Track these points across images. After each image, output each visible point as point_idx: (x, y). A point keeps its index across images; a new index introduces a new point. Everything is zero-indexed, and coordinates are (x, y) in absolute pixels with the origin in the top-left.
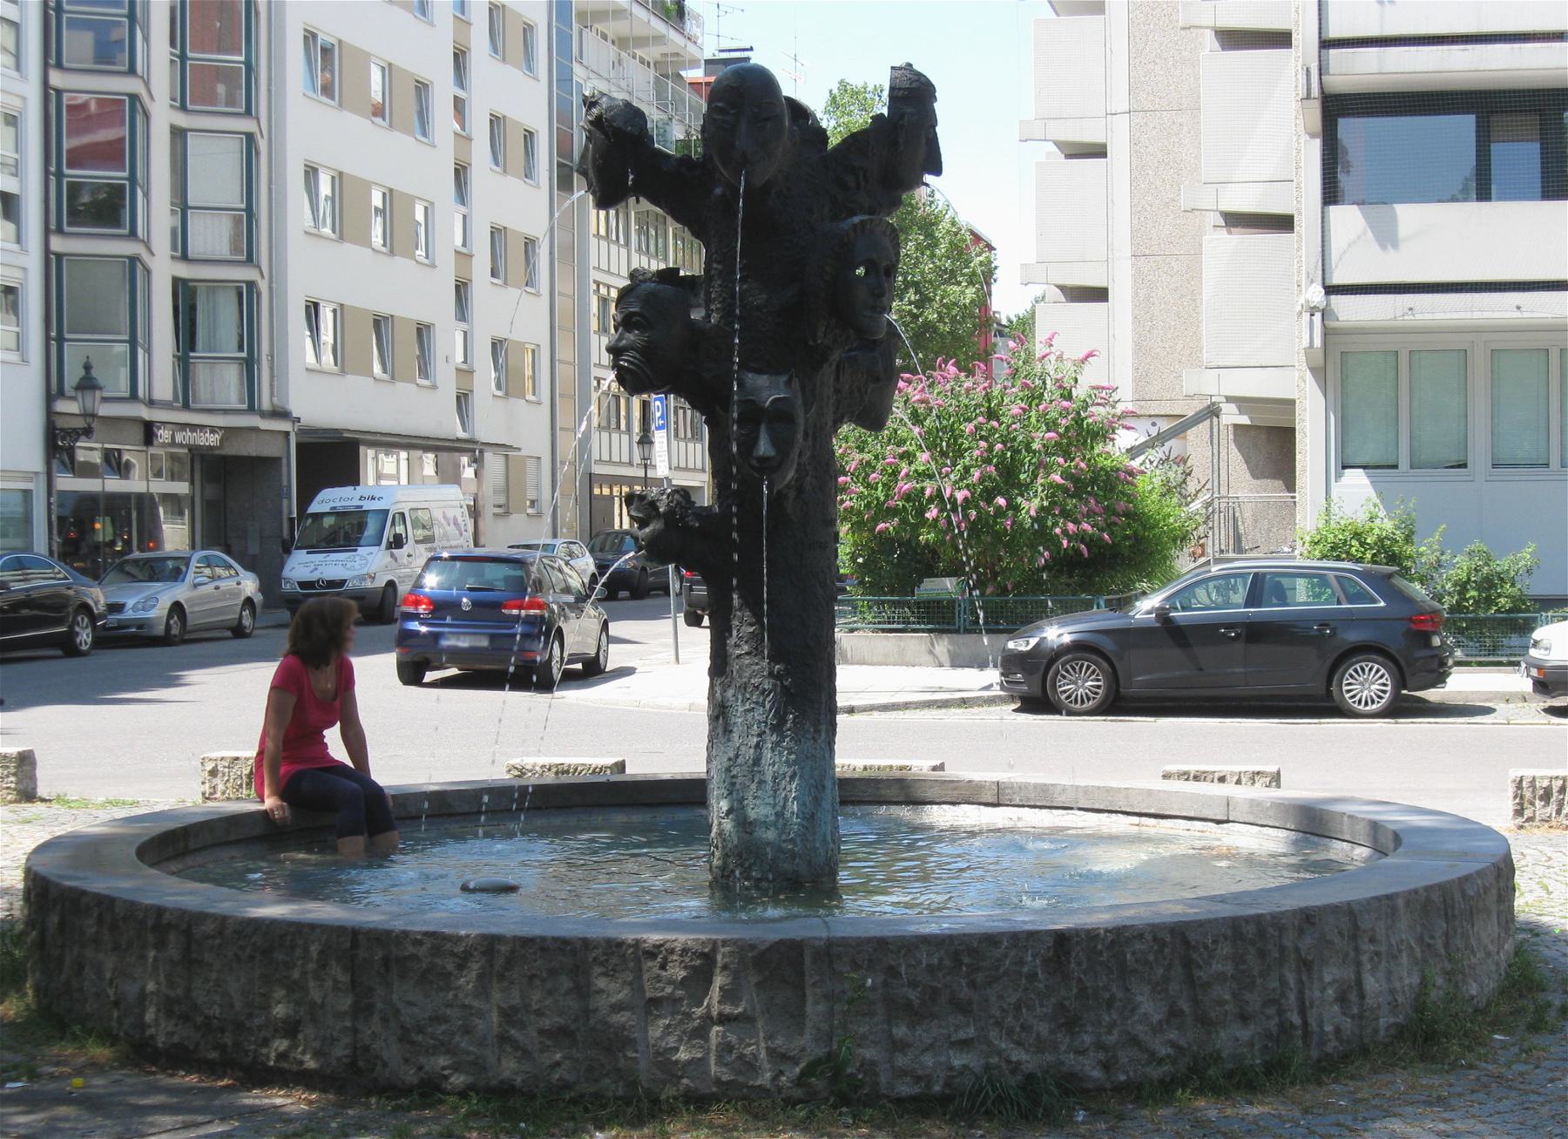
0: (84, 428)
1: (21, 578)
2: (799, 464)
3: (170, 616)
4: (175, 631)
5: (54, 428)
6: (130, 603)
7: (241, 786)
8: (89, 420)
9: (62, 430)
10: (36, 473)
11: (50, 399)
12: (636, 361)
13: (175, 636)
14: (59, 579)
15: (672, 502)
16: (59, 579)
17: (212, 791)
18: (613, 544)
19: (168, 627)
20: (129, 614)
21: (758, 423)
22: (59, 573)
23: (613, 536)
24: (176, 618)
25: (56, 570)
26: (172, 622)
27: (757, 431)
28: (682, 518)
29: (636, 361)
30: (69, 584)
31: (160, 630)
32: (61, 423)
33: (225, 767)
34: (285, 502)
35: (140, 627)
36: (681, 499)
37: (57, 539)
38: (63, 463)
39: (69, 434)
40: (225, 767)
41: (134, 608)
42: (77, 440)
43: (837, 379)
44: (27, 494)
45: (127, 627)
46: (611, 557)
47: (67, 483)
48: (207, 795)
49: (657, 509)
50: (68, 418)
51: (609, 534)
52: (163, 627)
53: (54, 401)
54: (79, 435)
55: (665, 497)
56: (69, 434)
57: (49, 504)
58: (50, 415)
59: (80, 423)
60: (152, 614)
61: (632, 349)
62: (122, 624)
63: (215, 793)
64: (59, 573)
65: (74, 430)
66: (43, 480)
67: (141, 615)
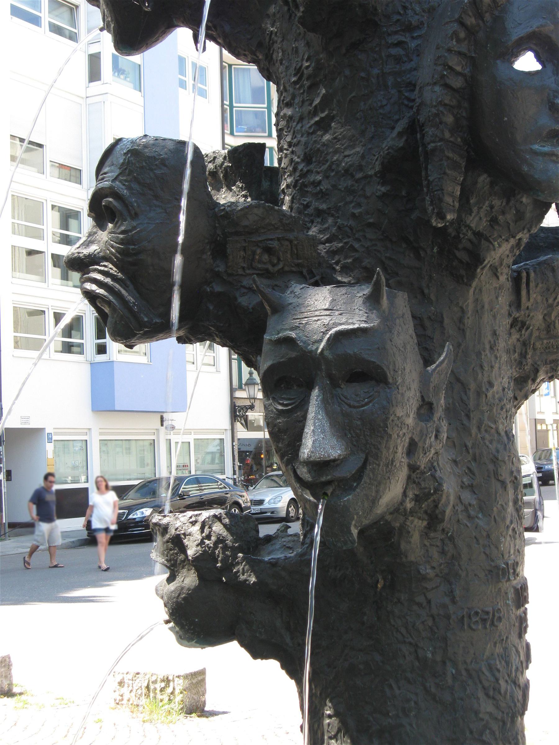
0: (250, 405)
1: (198, 488)
2: (413, 468)
3: (289, 506)
4: (292, 514)
5: (235, 406)
6: (267, 499)
7: (141, 695)
8: (252, 401)
9: (239, 406)
10: (226, 430)
11: (232, 391)
12: (108, 280)
13: (292, 517)
14: (221, 488)
15: (209, 537)
16: (221, 488)
17: (121, 698)
18: (546, 456)
19: (288, 512)
20: (266, 506)
21: (311, 388)
22: (221, 484)
23: (546, 451)
24: (292, 506)
25: (219, 484)
26: (290, 509)
27: (303, 405)
28: (228, 567)
29: (108, 280)
30: (226, 491)
31: (283, 514)
32: (239, 403)
33: (129, 680)
34: (6, 491)
35: (272, 513)
36: (224, 533)
37: (237, 463)
38: (242, 424)
39: (242, 409)
40: (129, 680)
41: (269, 502)
42: (246, 412)
43: (517, 303)
44: (222, 440)
45: (266, 513)
46: (545, 463)
47: (243, 433)
48: (117, 701)
49: (183, 549)
50: (243, 400)
51: (543, 451)
52: (285, 512)
53: (235, 392)
54: (247, 409)
55: (197, 527)
56: (242, 409)
57: (233, 446)
58: (232, 398)
59: (248, 403)
60: (279, 505)
61: (106, 258)
62: (263, 511)
63: (122, 700)
64: (221, 484)
65: (245, 406)
66: (229, 433)
67: (272, 506)
